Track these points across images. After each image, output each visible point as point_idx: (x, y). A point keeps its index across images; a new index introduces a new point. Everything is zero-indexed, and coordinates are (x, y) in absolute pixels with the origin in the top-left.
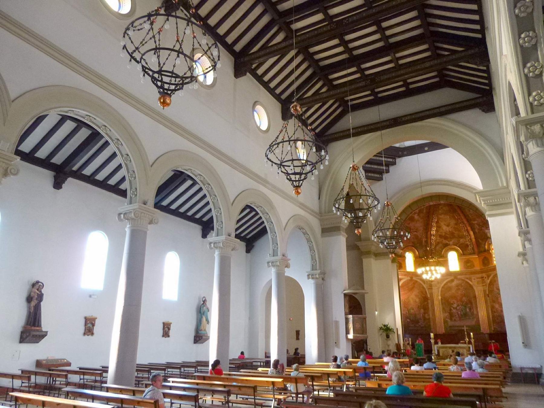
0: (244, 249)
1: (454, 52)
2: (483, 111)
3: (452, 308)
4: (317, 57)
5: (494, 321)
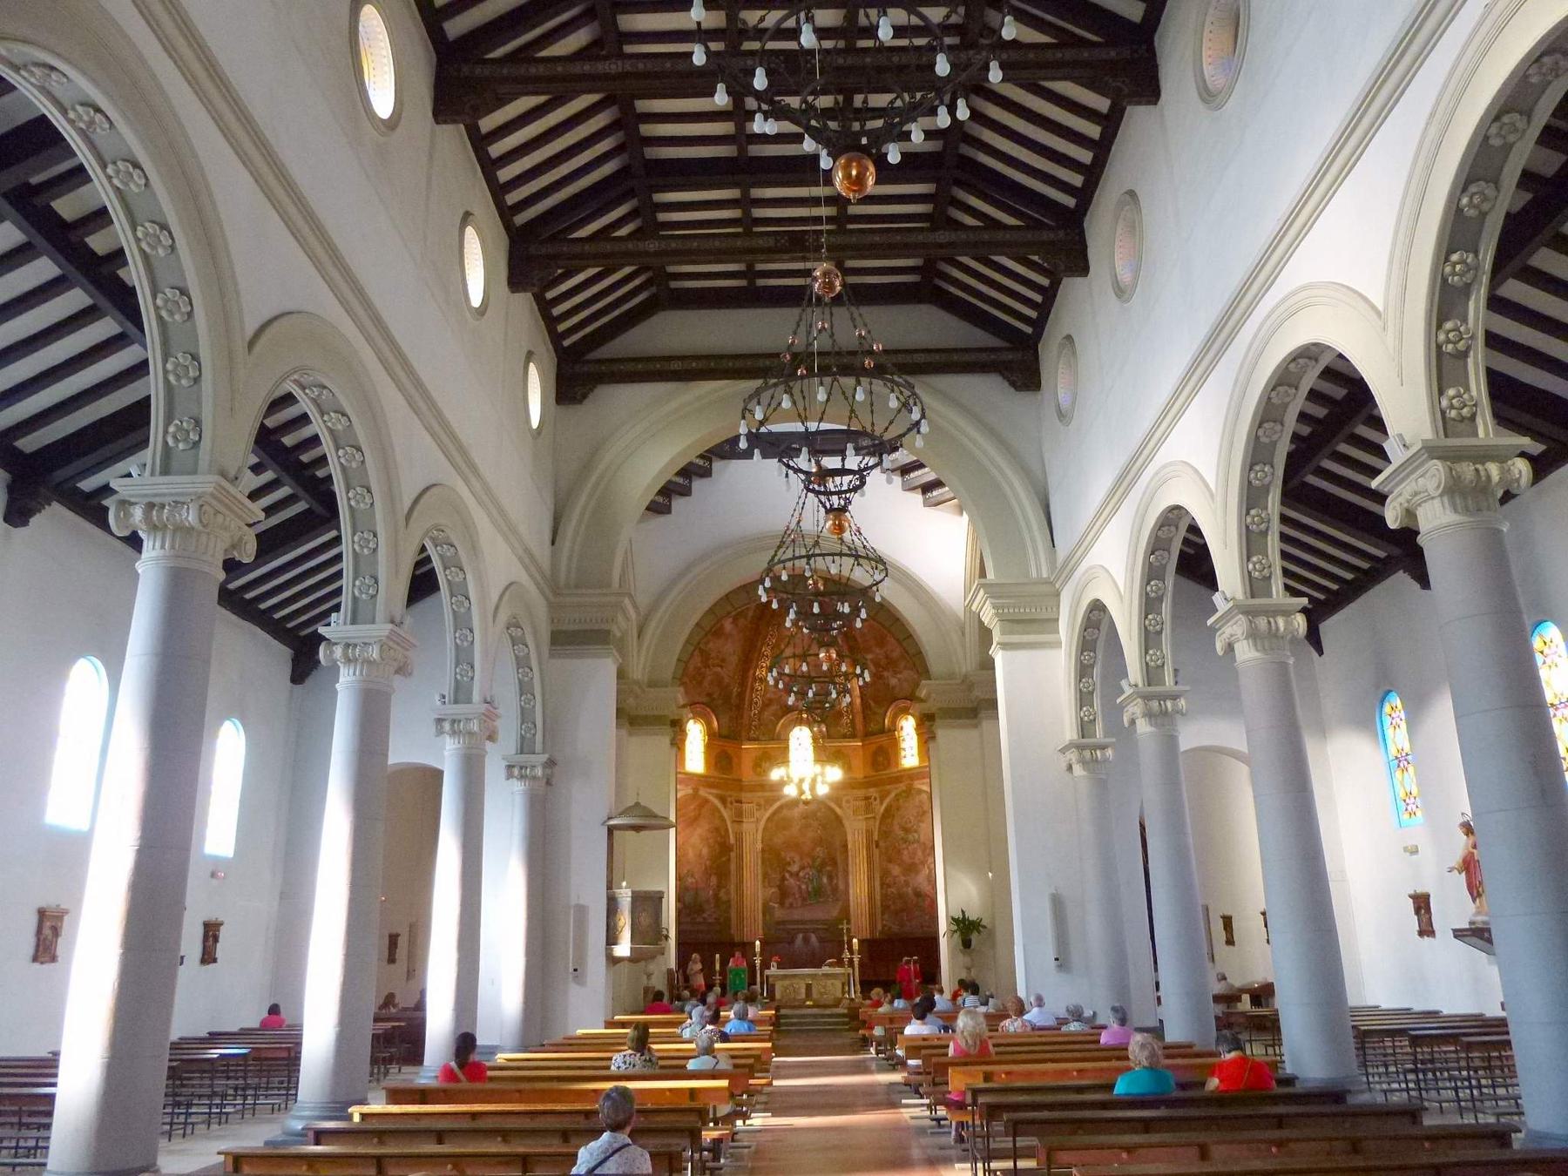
0: (286, 670)
1: (996, 225)
2: (1013, 384)
3: (787, 875)
4: (648, 129)
5: (885, 908)
